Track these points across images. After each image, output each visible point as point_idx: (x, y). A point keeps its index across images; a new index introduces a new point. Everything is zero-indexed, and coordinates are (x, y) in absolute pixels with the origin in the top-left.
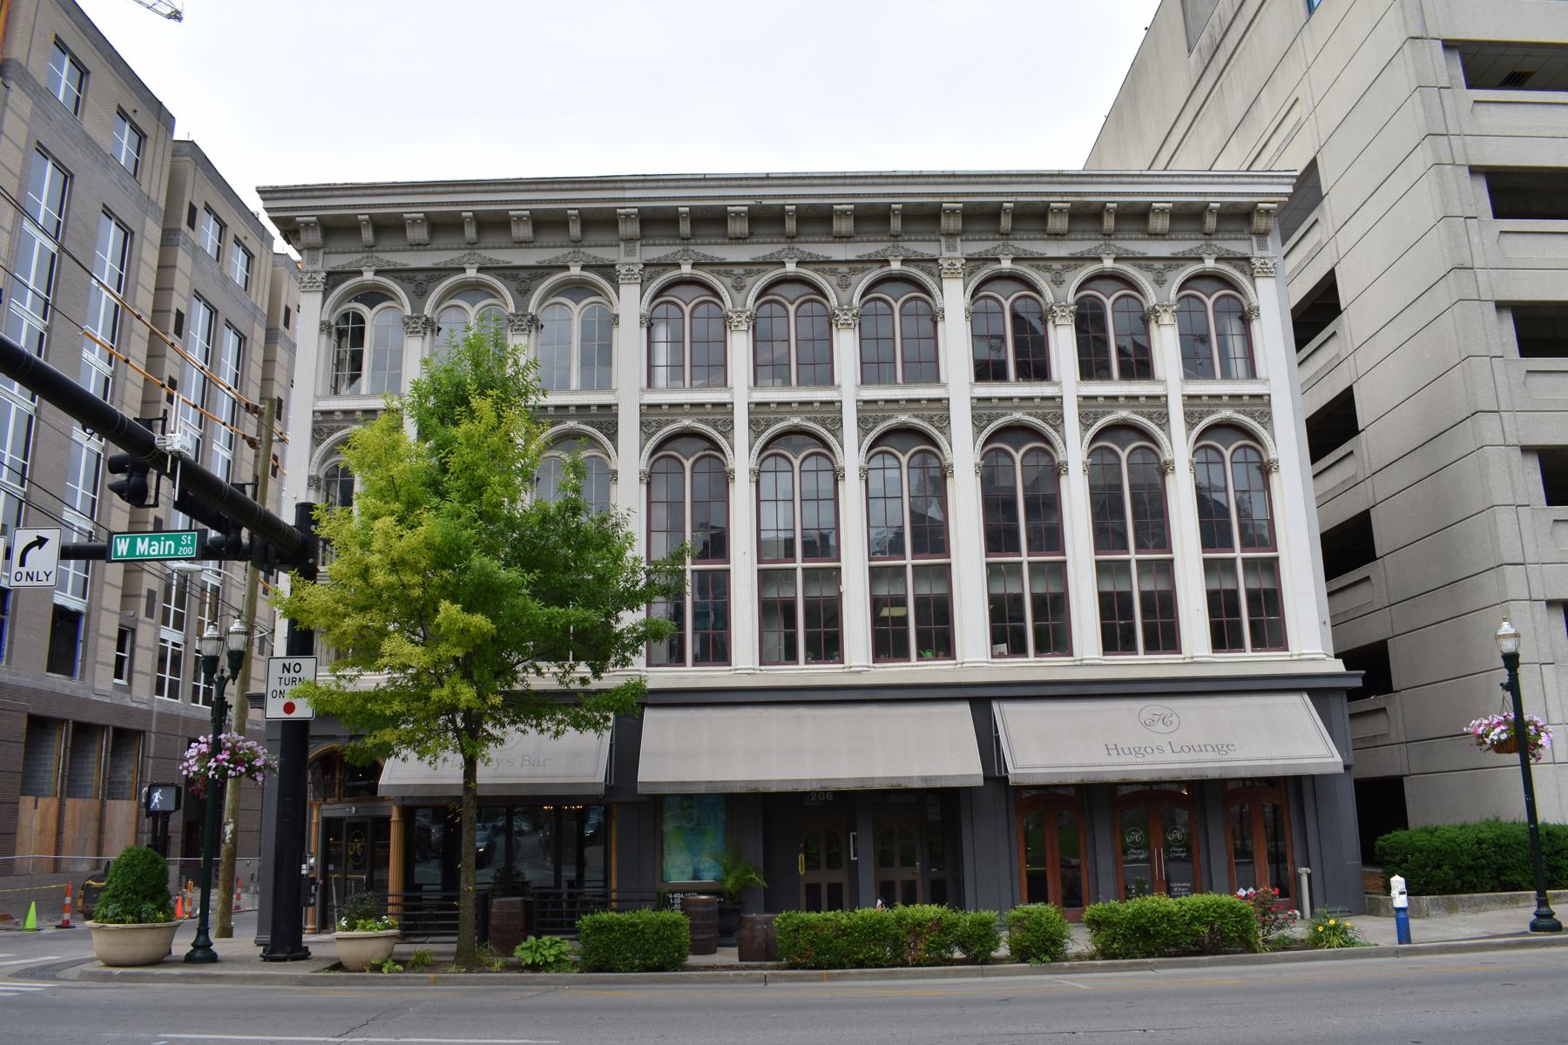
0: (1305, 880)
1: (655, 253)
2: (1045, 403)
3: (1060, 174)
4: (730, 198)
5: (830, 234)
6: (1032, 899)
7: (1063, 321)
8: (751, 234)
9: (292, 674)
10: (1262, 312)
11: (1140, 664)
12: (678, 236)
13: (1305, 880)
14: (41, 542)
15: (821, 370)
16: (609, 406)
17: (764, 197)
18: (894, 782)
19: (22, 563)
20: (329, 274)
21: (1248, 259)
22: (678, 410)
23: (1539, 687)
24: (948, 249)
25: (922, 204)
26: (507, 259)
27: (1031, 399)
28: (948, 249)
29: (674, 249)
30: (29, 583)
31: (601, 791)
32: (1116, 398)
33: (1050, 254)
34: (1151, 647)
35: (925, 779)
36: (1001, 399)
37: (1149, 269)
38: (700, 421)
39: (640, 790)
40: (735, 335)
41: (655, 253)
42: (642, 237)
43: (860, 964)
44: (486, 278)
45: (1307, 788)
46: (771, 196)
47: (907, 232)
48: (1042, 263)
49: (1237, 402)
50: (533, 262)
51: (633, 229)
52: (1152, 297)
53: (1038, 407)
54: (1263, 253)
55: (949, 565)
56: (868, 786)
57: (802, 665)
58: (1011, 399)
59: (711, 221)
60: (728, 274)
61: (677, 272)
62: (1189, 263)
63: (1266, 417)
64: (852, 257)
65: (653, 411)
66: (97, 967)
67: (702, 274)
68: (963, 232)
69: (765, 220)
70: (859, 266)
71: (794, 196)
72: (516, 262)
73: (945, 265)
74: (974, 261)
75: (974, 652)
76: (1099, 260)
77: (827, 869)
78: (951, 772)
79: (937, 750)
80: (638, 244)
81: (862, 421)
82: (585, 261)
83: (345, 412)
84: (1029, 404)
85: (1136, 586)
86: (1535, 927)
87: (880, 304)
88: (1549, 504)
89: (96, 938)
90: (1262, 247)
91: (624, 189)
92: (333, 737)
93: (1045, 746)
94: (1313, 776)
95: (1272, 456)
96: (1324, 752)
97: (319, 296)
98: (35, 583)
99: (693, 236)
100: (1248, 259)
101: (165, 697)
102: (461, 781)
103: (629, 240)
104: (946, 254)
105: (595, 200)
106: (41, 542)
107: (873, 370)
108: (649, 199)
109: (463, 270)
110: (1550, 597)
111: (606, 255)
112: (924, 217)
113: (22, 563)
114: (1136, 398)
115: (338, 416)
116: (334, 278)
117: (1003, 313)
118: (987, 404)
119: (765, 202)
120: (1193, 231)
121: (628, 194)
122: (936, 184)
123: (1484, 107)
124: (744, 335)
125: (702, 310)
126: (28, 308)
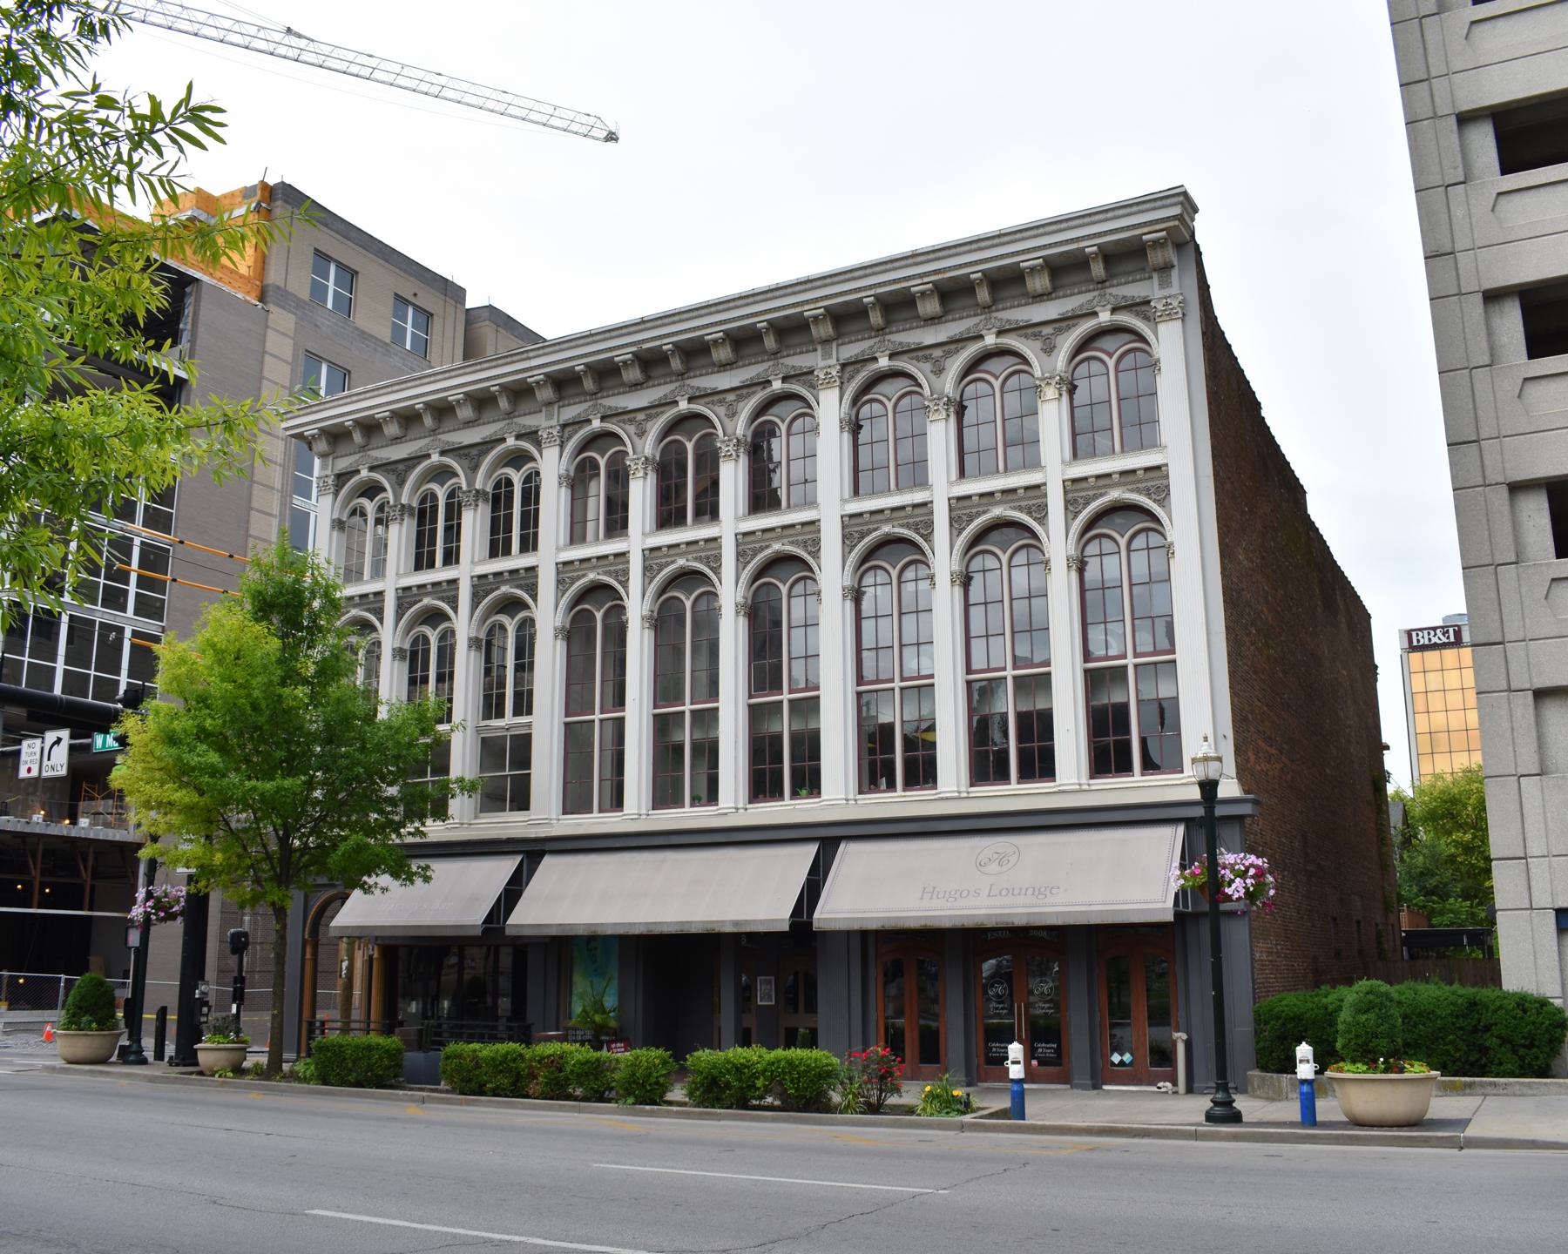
0: (1181, 1049)
1: (851, 351)
2: (917, 511)
3: (914, 255)
5: (1026, 295)
7: (936, 416)
8: (995, 301)
10: (1162, 365)
11: (1014, 795)
12: (585, 393)
13: (1181, 1049)
15: (1024, 447)
17: (643, 341)
18: (709, 926)
20: (844, 366)
22: (879, 517)
23: (1515, 807)
24: (824, 358)
25: (786, 317)
27: (903, 508)
28: (824, 358)
31: (478, 932)
32: (991, 494)
33: (927, 342)
34: (1026, 774)
35: (736, 923)
36: (872, 513)
38: (1132, 491)
39: (508, 932)
40: (934, 425)
41: (851, 351)
42: (560, 399)
44: (447, 460)
46: (648, 339)
47: (742, 358)
48: (920, 354)
49: (1130, 478)
51: (825, 330)
54: (1165, 293)
55: (1049, 674)
56: (657, 930)
57: (899, 792)
58: (881, 511)
59: (898, 306)
60: (927, 358)
62: (1082, 321)
64: (736, 384)
65: (568, 568)
66: (60, 1063)
67: (900, 364)
69: (651, 363)
70: (744, 391)
71: (669, 335)
72: (395, 457)
73: (1160, 307)
75: (840, 791)
76: (1095, 314)
77: (709, 1014)
78: (761, 916)
79: (749, 894)
80: (834, 345)
81: (647, 569)
82: (518, 430)
84: (902, 514)
85: (785, 726)
86: (1210, 1118)
87: (980, 385)
88: (1558, 557)
89: (59, 1042)
90: (1165, 283)
93: (878, 890)
97: (557, 449)
99: (995, 301)
101: (899, 792)
103: (549, 404)
104: (822, 364)
105: (686, 331)
106: (59, 741)
107: (1081, 443)
108: (681, 332)
110: (1540, 683)
112: (792, 331)
114: (1014, 491)
116: (342, 478)
118: (859, 520)
119: (645, 346)
121: (534, 363)
122: (1154, 209)
123: (1487, 26)
124: (942, 424)
125: (1129, 361)
126: (137, 541)
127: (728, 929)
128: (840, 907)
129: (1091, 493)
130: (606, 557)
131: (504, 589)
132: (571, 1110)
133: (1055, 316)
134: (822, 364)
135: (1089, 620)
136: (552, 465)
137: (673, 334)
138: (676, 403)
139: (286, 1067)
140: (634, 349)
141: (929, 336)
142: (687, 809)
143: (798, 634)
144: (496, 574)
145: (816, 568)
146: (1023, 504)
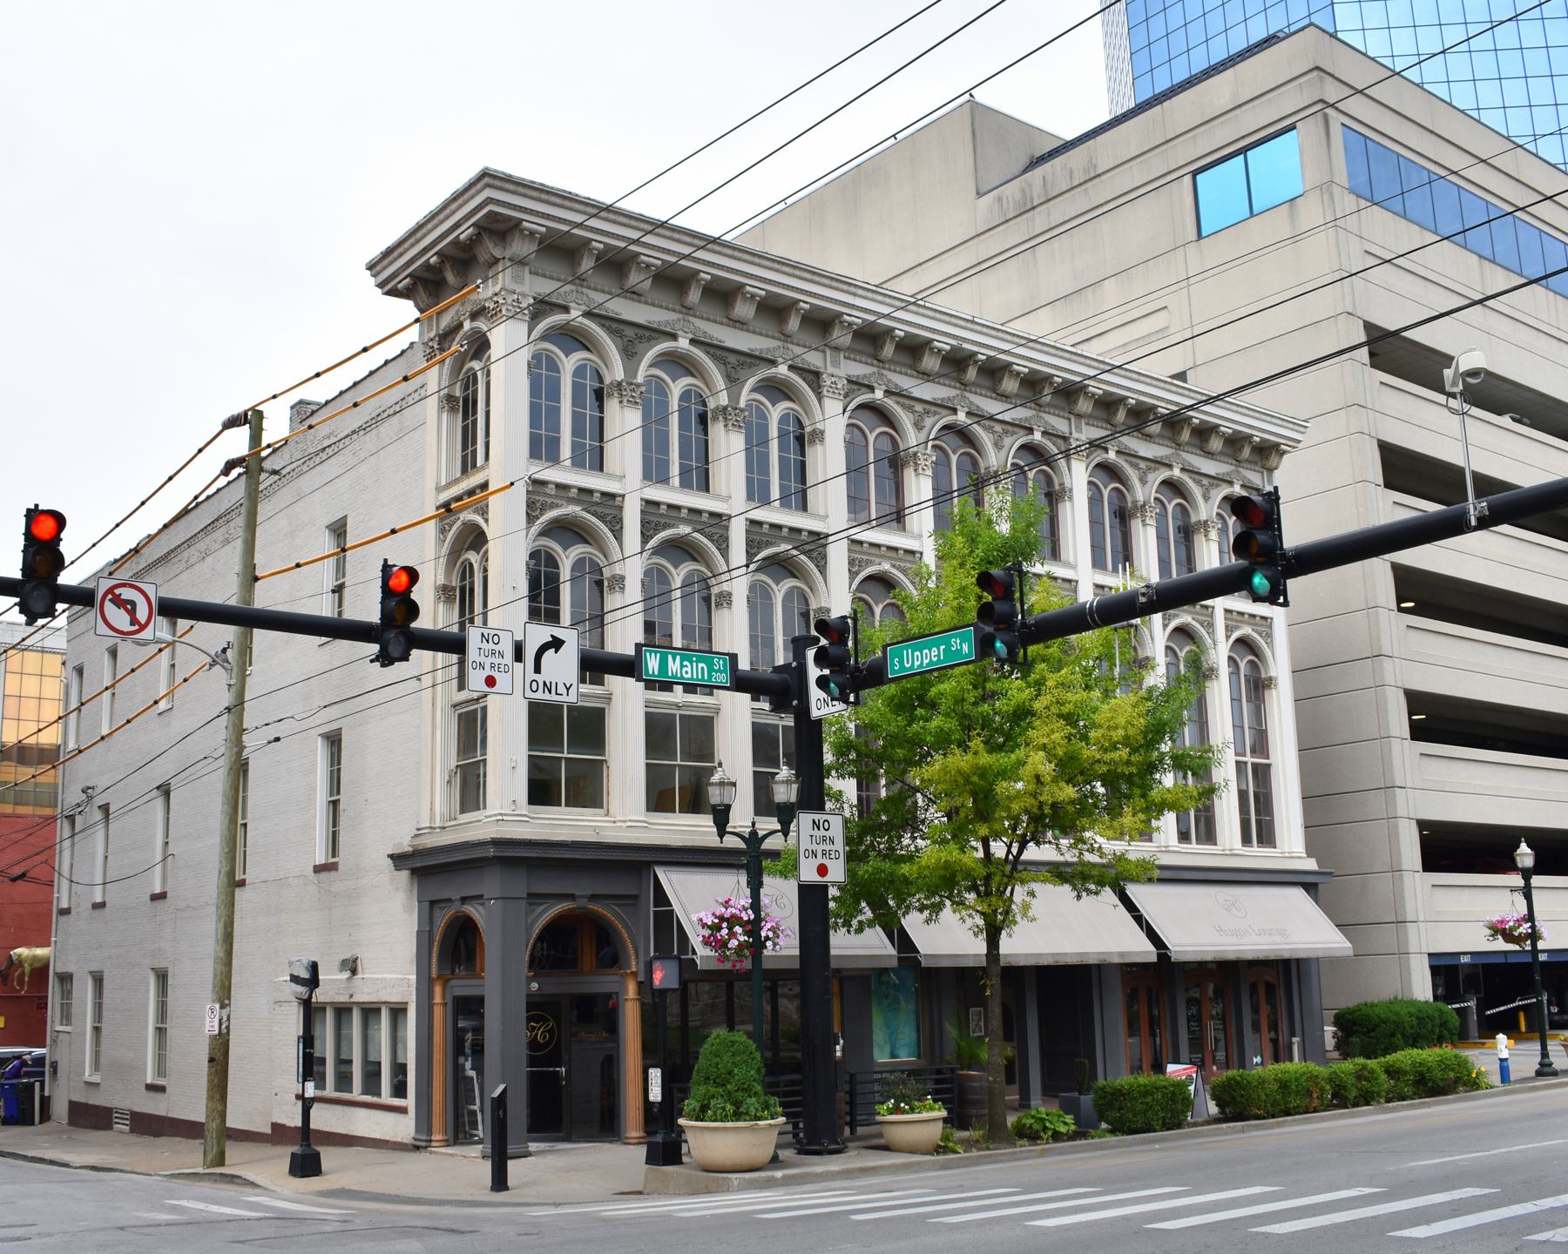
4: (751, 276)
6: (1277, 1060)
9: (822, 832)
14: (556, 644)
16: (612, 496)
19: (537, 670)
21: (817, 374)
26: (617, 309)
29: (672, 316)
30: (547, 696)
35: (1121, 954)
37: (910, 409)
39: (834, 965)
43: (1288, 1113)
44: (698, 353)
45: (1095, 974)
50: (744, 348)
52: (912, 438)
53: (597, 504)
56: (1062, 961)
61: (871, 396)
63: (1269, 636)
67: (891, 403)
68: (1090, 416)
72: (729, 343)
74: (855, 384)
76: (674, 337)
83: (559, 486)
91: (855, 295)
92: (572, 897)
94: (1298, 960)
95: (1272, 673)
96: (878, 943)
98: (554, 697)
99: (891, 361)
100: (817, 374)
102: (797, 952)
104: (831, 370)
106: (556, 644)
109: (773, 363)
111: (814, 359)
113: (537, 670)
115: (551, 490)
117: (949, 466)
119: (965, 346)
120: (904, 365)
127: (1116, 960)
128: (1019, 945)
129: (549, 500)
130: (896, 549)
131: (784, 547)
132: (1257, 1128)
133: (929, 398)
134: (831, 370)
135: (324, 608)
136: (1077, 476)
137: (722, 267)
138: (871, 389)
139: (1011, 1120)
140: (954, 342)
141: (1209, 467)
142: (1255, 848)
143: (183, 565)
144: (560, 487)
145: (1268, 652)
146: (599, 510)
